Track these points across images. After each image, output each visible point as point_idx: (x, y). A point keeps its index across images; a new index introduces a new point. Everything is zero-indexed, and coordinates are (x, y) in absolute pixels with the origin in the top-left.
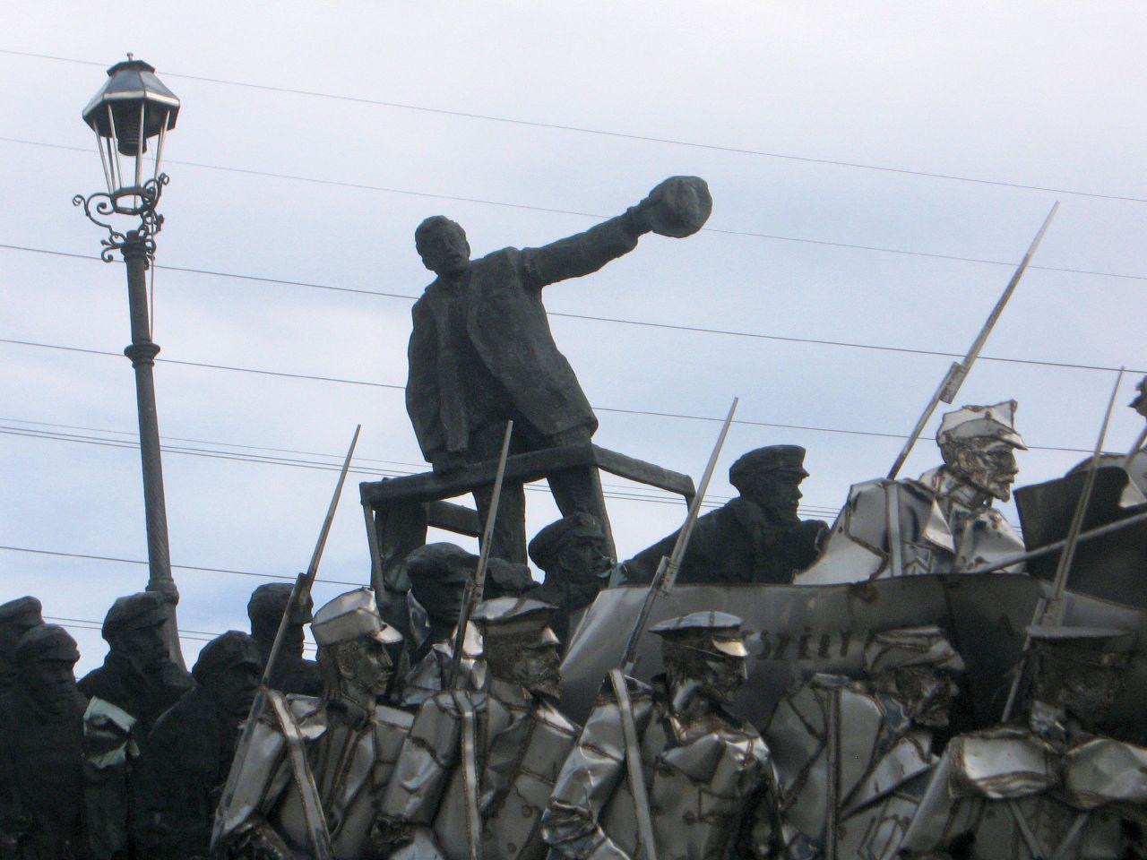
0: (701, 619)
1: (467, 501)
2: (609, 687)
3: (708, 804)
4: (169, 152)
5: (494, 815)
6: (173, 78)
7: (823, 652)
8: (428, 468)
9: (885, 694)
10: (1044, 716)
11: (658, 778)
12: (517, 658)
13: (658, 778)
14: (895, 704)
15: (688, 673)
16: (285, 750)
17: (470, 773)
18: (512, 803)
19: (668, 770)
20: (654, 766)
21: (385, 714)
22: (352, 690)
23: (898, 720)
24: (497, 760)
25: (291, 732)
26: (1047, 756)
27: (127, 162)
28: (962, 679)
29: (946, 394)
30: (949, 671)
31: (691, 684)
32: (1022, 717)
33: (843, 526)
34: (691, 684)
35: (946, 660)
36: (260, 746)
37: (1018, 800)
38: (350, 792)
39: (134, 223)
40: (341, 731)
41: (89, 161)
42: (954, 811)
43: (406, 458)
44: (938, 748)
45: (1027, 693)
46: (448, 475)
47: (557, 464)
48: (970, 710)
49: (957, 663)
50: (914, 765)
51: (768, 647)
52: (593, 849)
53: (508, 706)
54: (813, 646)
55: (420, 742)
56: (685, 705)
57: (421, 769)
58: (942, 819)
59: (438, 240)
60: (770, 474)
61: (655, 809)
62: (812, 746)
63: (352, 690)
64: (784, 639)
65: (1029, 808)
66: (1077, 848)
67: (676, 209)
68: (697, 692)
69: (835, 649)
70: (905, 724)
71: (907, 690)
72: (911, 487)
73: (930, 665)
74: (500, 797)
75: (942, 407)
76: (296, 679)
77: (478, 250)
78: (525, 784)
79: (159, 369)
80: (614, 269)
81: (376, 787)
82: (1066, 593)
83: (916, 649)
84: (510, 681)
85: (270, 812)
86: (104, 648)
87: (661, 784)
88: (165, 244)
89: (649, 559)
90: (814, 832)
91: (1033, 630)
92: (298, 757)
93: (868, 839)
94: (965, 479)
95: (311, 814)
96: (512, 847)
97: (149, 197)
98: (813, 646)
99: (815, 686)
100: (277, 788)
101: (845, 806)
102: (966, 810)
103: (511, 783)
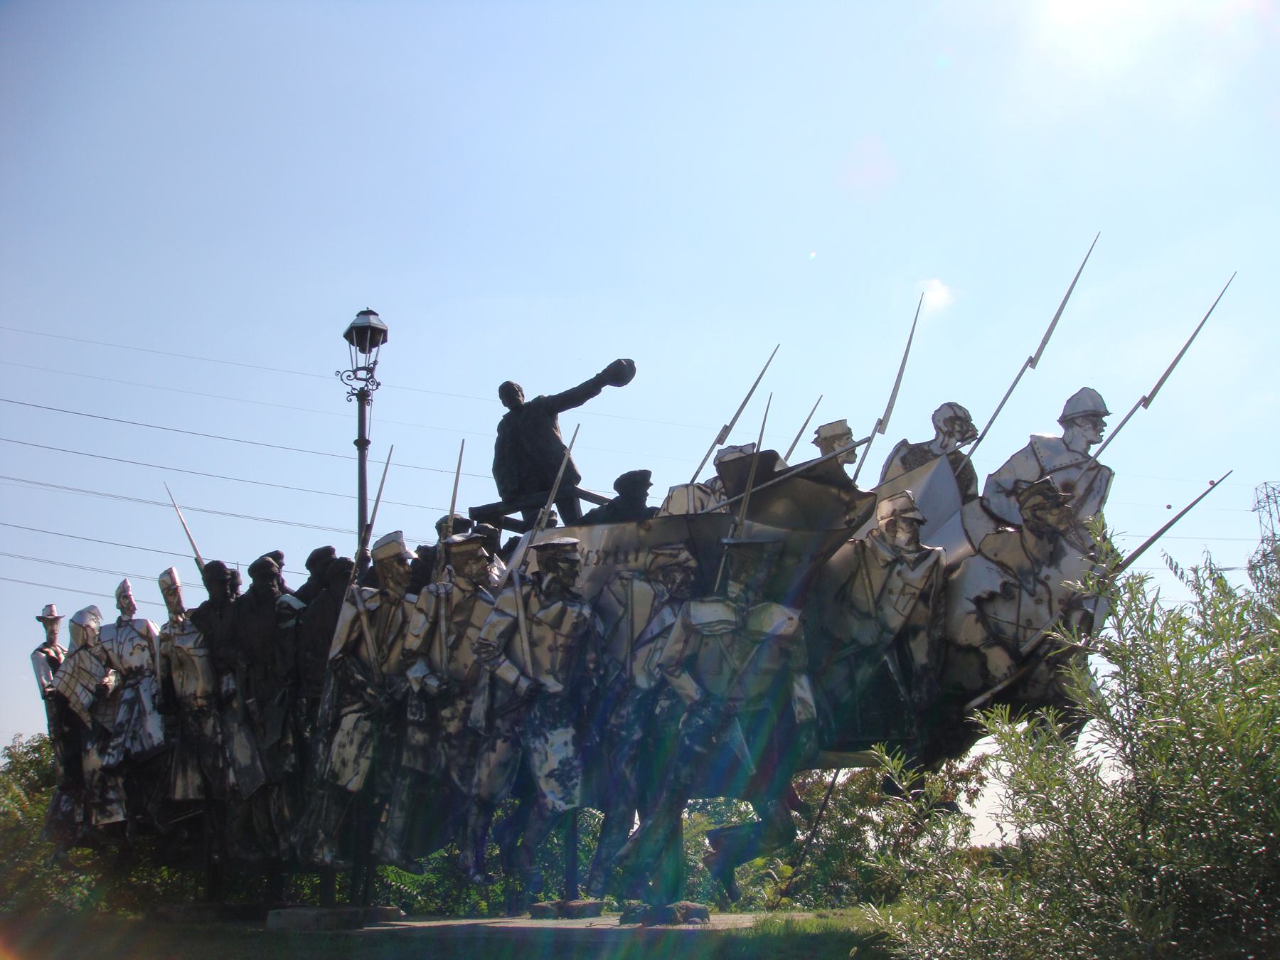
1: (518, 516)
3: (561, 641)
4: (383, 353)
5: (457, 648)
6: (384, 319)
7: (626, 561)
8: (500, 500)
9: (657, 581)
10: (734, 589)
11: (535, 628)
12: (466, 564)
13: (535, 628)
14: (661, 587)
16: (357, 618)
17: (443, 624)
18: (466, 644)
19: (539, 623)
20: (531, 619)
22: (391, 584)
23: (663, 596)
26: (735, 611)
27: (362, 356)
29: (720, 440)
30: (690, 568)
32: (724, 587)
34: (550, 576)
36: (347, 612)
37: (721, 636)
38: (391, 639)
39: (362, 384)
40: (386, 606)
41: (346, 355)
42: (686, 642)
45: (726, 578)
46: (510, 502)
48: (701, 586)
49: (693, 563)
51: (599, 559)
52: (500, 665)
53: (463, 591)
55: (420, 610)
56: (548, 587)
57: (418, 624)
58: (679, 646)
59: (509, 393)
60: (634, 484)
61: (533, 644)
62: (621, 611)
63: (391, 584)
67: (620, 373)
68: (553, 580)
69: (631, 557)
70: (667, 597)
73: (679, 564)
74: (460, 638)
75: (718, 447)
78: (471, 632)
79: (371, 452)
82: (746, 522)
84: (464, 577)
85: (352, 648)
88: (376, 396)
90: (622, 658)
95: (369, 650)
96: (465, 666)
98: (622, 557)
99: (621, 578)
100: (355, 635)
101: (637, 644)
102: (693, 641)
103: (465, 632)
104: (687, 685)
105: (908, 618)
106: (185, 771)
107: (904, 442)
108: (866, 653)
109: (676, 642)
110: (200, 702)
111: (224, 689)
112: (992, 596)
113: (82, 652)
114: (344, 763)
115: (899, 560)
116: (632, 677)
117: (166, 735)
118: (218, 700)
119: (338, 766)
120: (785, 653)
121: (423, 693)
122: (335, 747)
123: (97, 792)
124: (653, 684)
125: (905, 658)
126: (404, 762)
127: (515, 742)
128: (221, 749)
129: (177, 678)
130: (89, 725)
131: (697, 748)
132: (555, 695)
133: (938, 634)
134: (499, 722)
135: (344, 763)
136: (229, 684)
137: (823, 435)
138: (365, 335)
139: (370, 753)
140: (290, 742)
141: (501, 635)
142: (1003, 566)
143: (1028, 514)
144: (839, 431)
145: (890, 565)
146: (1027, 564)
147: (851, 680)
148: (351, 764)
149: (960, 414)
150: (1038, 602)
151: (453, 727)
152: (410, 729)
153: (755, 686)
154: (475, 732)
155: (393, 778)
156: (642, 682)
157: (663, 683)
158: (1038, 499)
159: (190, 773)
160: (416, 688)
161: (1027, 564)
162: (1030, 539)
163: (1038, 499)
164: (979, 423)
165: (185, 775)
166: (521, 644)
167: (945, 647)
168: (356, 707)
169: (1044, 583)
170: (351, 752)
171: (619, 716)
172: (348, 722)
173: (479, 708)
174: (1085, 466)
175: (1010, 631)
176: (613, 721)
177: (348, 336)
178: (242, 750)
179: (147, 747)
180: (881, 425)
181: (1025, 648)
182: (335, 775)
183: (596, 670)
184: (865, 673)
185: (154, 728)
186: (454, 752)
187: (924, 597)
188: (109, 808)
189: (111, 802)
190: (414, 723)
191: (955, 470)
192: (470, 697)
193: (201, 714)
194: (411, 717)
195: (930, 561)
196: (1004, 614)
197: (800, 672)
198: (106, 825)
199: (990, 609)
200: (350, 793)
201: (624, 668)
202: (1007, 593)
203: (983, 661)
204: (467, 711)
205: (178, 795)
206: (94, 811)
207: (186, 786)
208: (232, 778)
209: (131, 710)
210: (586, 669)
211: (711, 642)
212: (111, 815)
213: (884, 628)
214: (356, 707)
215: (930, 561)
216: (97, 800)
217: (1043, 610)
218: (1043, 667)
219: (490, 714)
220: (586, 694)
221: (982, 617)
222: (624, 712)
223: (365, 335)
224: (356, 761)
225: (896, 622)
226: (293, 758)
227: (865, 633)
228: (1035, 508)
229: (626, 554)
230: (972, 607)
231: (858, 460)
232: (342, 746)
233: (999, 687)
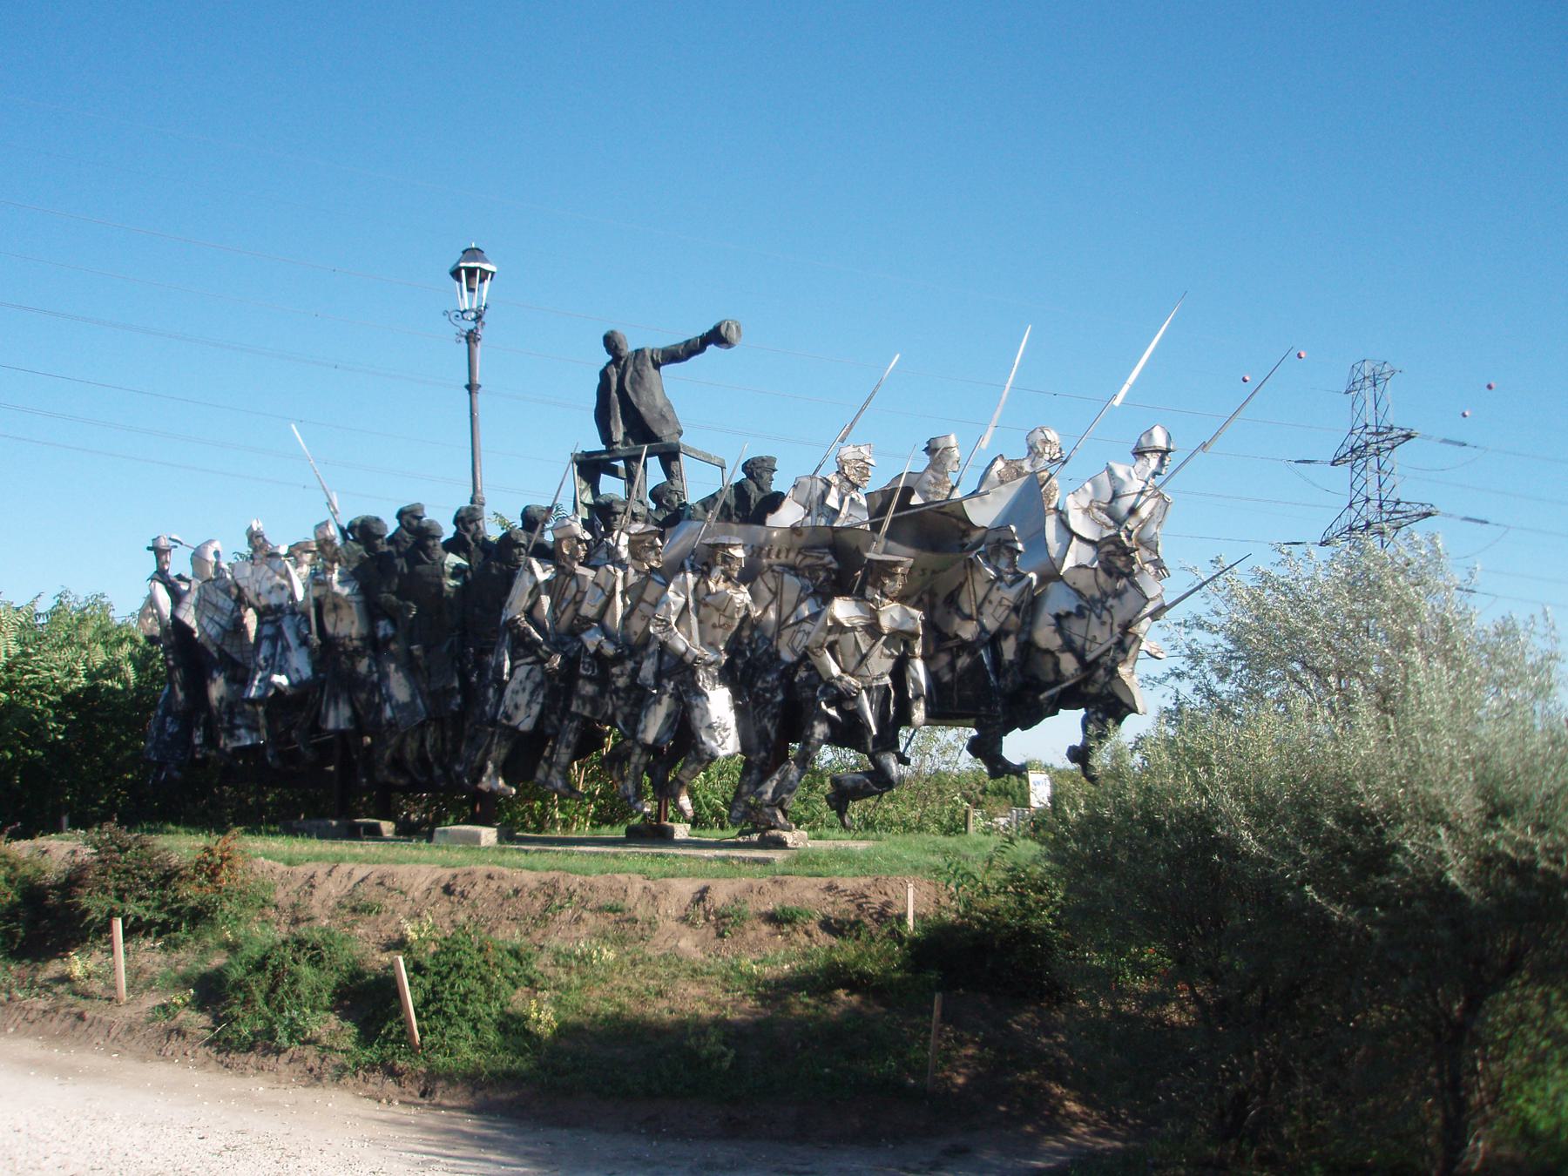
14: (807, 582)
18: (637, 612)
28: (837, 572)
35: (483, 1138)
39: (472, 325)
43: (593, 442)
48: (840, 585)
49: (835, 566)
60: (756, 469)
67: (717, 337)
69: (783, 555)
73: (824, 566)
76: (545, 553)
77: (629, 346)
86: (454, 529)
87: (703, 610)
89: (707, 503)
91: (869, 555)
93: (792, 639)
106: (337, 704)
108: (965, 646)
110: (356, 643)
111: (381, 633)
112: (1069, 614)
114: (517, 707)
116: (778, 652)
117: (313, 670)
118: (374, 645)
121: (598, 654)
125: (997, 655)
126: (573, 709)
128: (376, 687)
129: (329, 622)
133: (1023, 637)
136: (384, 628)
139: (540, 699)
140: (456, 684)
142: (1079, 593)
145: (992, 582)
146: (1097, 595)
147: (952, 666)
148: (523, 708)
150: (1103, 623)
151: (621, 682)
152: (581, 682)
155: (561, 721)
159: (341, 705)
161: (1097, 595)
163: (1111, 548)
165: (337, 707)
167: (1028, 648)
168: (529, 660)
169: (1108, 610)
170: (523, 698)
171: (765, 681)
173: (648, 668)
175: (1079, 642)
176: (759, 684)
178: (399, 688)
181: (1090, 657)
182: (508, 717)
183: (749, 644)
184: (964, 661)
186: (621, 703)
187: (1016, 609)
189: (239, 727)
193: (356, 653)
194: (583, 672)
195: (1024, 583)
196: (1076, 628)
198: (235, 749)
199: (1066, 624)
200: (523, 733)
202: (1080, 613)
203: (1057, 663)
204: (635, 672)
205: (331, 725)
207: (337, 717)
208: (388, 712)
209: (275, 646)
212: (239, 739)
213: (983, 628)
214: (529, 660)
215: (1024, 583)
218: (1101, 672)
224: (529, 704)
226: (459, 699)
227: (968, 631)
228: (1109, 553)
230: (1053, 621)
232: (515, 692)
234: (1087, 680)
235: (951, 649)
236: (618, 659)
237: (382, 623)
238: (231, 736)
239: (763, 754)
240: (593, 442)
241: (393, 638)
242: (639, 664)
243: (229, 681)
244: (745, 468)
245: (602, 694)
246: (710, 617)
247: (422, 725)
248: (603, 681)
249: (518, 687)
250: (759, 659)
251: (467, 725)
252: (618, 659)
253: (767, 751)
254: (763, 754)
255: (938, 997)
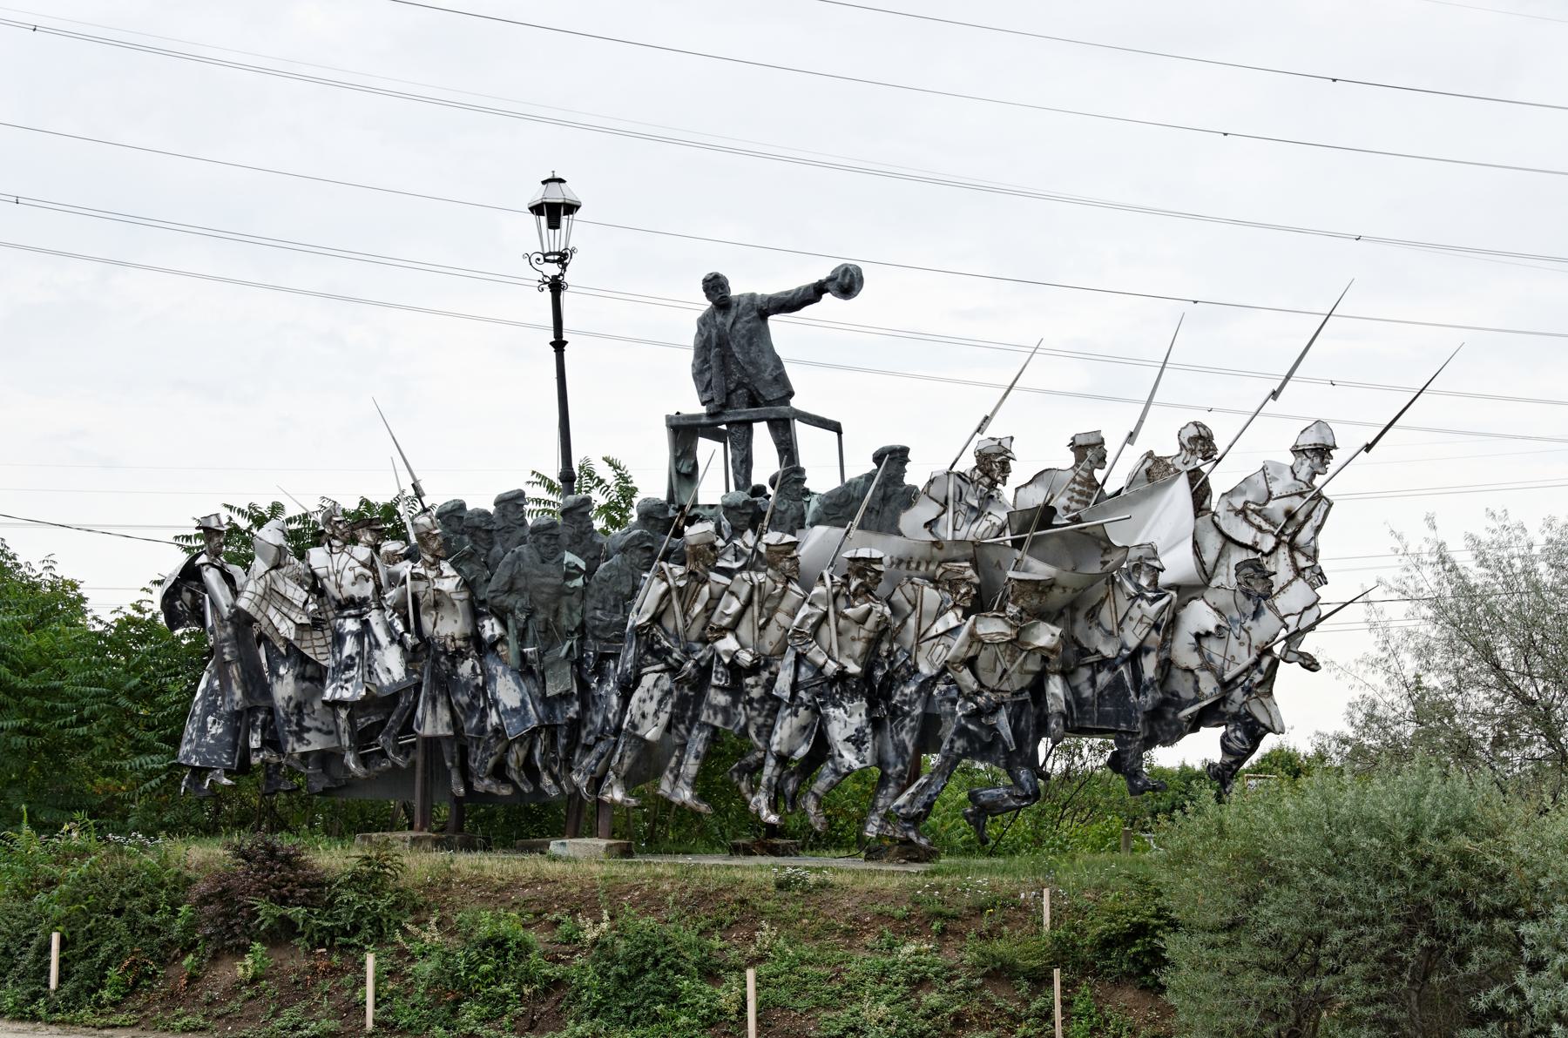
0: (863, 553)
2: (822, 578)
3: (863, 633)
4: (574, 230)
8: (703, 410)
10: (1012, 610)
14: (947, 595)
15: (859, 576)
16: (668, 591)
18: (773, 626)
19: (846, 617)
21: (714, 576)
24: (767, 605)
25: (671, 581)
28: (978, 587)
29: (979, 430)
31: (859, 581)
32: (1003, 609)
33: (926, 492)
34: (859, 581)
40: (694, 584)
41: (531, 233)
43: (692, 404)
44: (966, 616)
47: (773, 416)
48: (979, 604)
49: (976, 580)
50: (953, 623)
54: (913, 565)
58: (965, 649)
59: (715, 286)
61: (839, 633)
62: (909, 608)
64: (900, 561)
65: (1002, 647)
66: (1021, 665)
67: (846, 284)
69: (922, 568)
71: (953, 586)
72: (960, 475)
77: (736, 289)
78: (781, 617)
79: (568, 351)
80: (807, 311)
81: (709, 609)
83: (958, 572)
85: (656, 619)
87: (842, 622)
92: (674, 594)
93: (931, 652)
94: (986, 474)
97: (562, 258)
98: (913, 565)
104: (966, 678)
105: (1143, 641)
107: (1150, 455)
108: (1105, 663)
109: (962, 645)
111: (487, 633)
112: (1208, 634)
113: (273, 572)
114: (644, 716)
115: (1141, 596)
117: (407, 670)
119: (637, 718)
120: (1045, 659)
122: (634, 701)
123: (294, 719)
124: (935, 672)
126: (703, 718)
127: (815, 711)
128: (482, 689)
129: (427, 622)
130: (283, 650)
131: (970, 727)
132: (853, 675)
133: (1163, 655)
134: (802, 694)
135: (644, 716)
136: (491, 629)
137: (1078, 442)
138: (554, 212)
139: (669, 708)
141: (813, 626)
143: (1242, 580)
144: (1093, 440)
145: (1133, 598)
148: (650, 718)
149: (1203, 433)
150: (1241, 644)
151: (756, 693)
152: (712, 692)
153: (1017, 682)
154: (779, 700)
156: (925, 669)
157: (944, 670)
158: (1250, 570)
160: (727, 660)
162: (1241, 598)
164: (1220, 443)
166: (828, 633)
168: (658, 667)
170: (651, 707)
172: (648, 681)
174: (1309, 496)
175: (1218, 661)
177: (531, 209)
178: (508, 692)
179: (386, 683)
180: (1131, 437)
181: (1227, 677)
182: (634, 726)
184: (1104, 678)
185: (391, 665)
186: (754, 713)
187: (1156, 627)
188: (306, 736)
189: (308, 730)
190: (716, 687)
191: (1192, 486)
192: (773, 669)
196: (1212, 646)
197: (1054, 673)
201: (910, 657)
204: (771, 683)
206: (291, 739)
208: (493, 718)
209: (360, 641)
210: (879, 656)
211: (991, 648)
212: (309, 743)
213: (1124, 646)
214: (658, 667)
216: (294, 728)
217: (1245, 649)
219: (795, 686)
220: (879, 673)
221: (1198, 648)
222: (907, 691)
223: (554, 212)
224: (656, 714)
225: (1133, 642)
226: (577, 706)
227: (1109, 650)
229: (919, 564)
231: (1107, 467)
233: (1206, 703)
234: (1223, 700)
235: (1091, 664)
236: (754, 669)
237: (487, 623)
238: (300, 739)
239: (900, 767)
240: (692, 404)
241: (502, 639)
242: (774, 677)
243: (300, 677)
244: (878, 458)
245: (734, 704)
246: (847, 630)
247: (534, 732)
248: (735, 689)
249: (646, 696)
250: (897, 671)
251: (584, 734)
252: (754, 669)
253: (904, 763)
254: (900, 767)
255: (1057, 972)
